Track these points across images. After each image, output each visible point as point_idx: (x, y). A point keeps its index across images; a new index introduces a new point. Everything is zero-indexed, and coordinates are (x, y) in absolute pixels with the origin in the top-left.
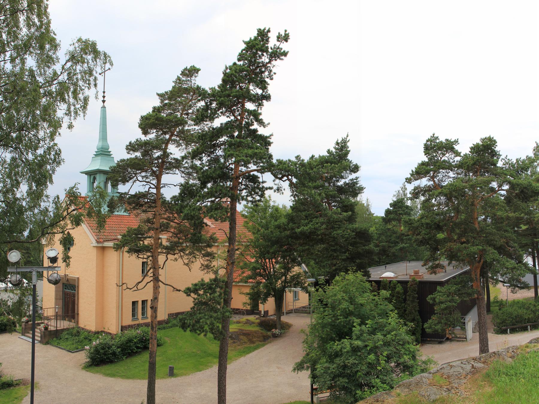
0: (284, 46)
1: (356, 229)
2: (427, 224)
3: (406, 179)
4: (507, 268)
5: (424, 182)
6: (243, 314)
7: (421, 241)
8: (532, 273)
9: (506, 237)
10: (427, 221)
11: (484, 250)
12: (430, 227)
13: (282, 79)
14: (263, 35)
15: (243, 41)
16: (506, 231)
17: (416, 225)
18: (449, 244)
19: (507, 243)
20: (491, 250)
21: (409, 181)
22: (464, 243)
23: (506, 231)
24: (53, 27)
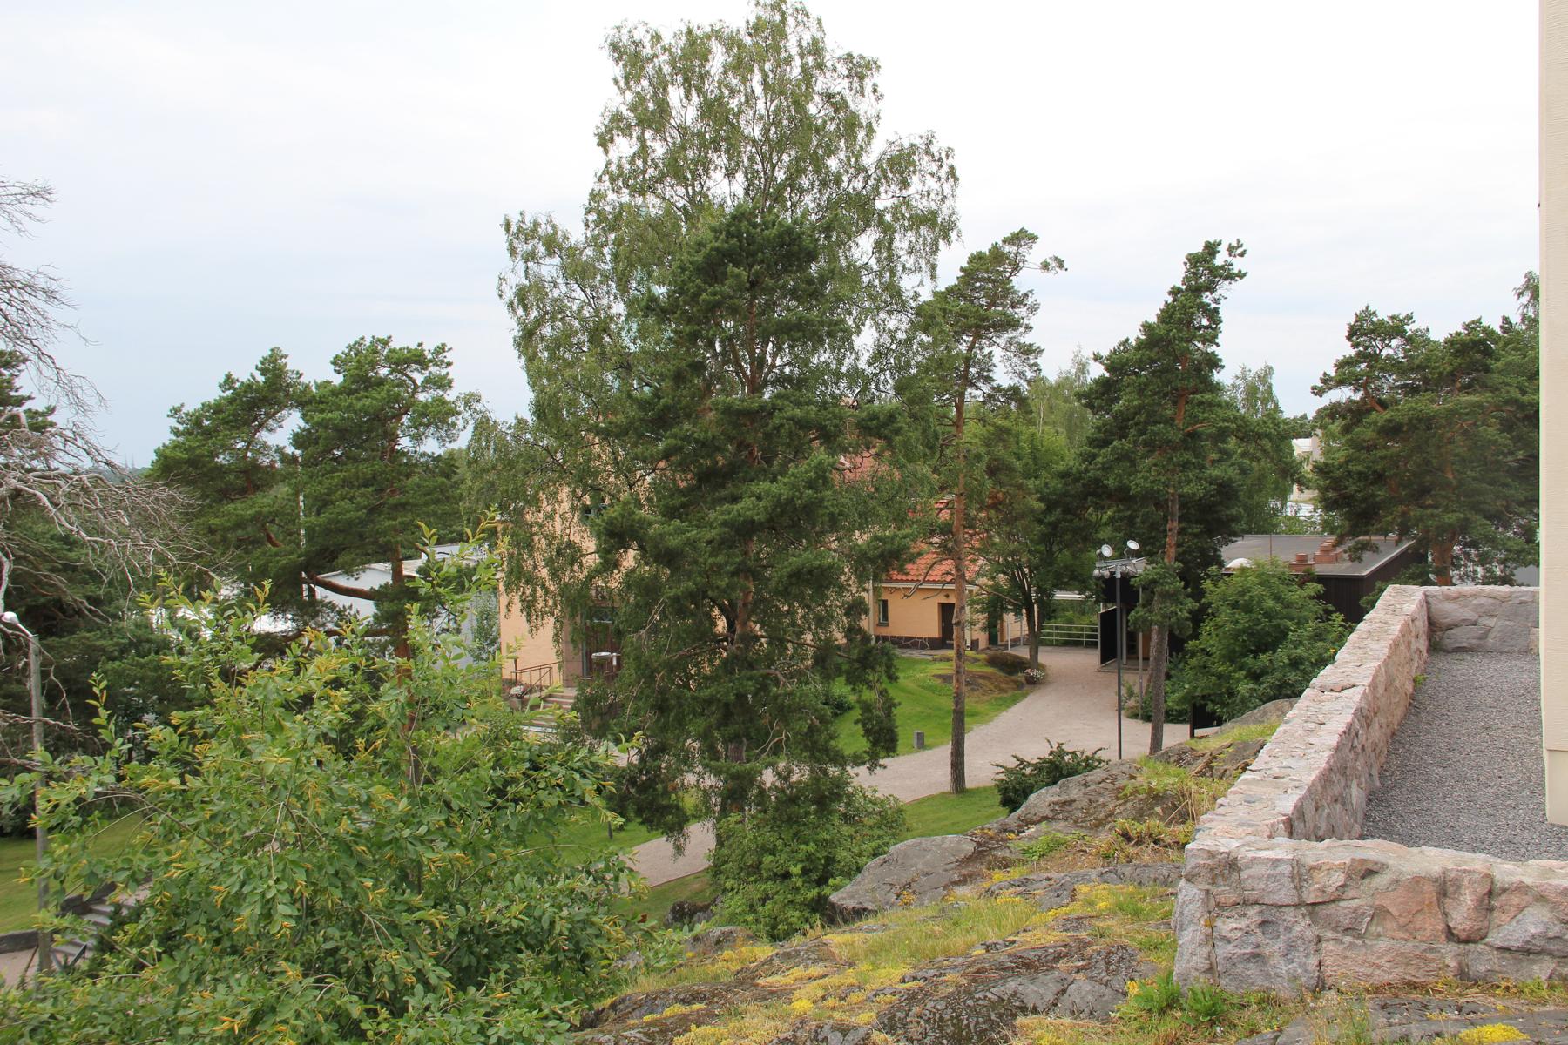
0: (1238, 264)
1: (1217, 478)
2: (1360, 473)
3: (1314, 388)
4: (1508, 551)
5: (1344, 394)
6: (923, 647)
7: (1335, 501)
8: (1463, 936)
9: (1505, 498)
10: (1360, 468)
11: (1466, 519)
12: (1366, 479)
13: (1230, 299)
14: (1211, 249)
15: (1207, 270)
16: (1505, 485)
17: (1337, 474)
18: (321, 448)
19: (1507, 507)
20: (1479, 519)
21: (1318, 392)
22: (1430, 506)
23: (1505, 485)
24: (1275, 390)
